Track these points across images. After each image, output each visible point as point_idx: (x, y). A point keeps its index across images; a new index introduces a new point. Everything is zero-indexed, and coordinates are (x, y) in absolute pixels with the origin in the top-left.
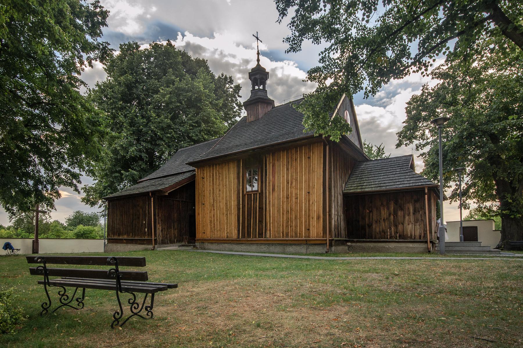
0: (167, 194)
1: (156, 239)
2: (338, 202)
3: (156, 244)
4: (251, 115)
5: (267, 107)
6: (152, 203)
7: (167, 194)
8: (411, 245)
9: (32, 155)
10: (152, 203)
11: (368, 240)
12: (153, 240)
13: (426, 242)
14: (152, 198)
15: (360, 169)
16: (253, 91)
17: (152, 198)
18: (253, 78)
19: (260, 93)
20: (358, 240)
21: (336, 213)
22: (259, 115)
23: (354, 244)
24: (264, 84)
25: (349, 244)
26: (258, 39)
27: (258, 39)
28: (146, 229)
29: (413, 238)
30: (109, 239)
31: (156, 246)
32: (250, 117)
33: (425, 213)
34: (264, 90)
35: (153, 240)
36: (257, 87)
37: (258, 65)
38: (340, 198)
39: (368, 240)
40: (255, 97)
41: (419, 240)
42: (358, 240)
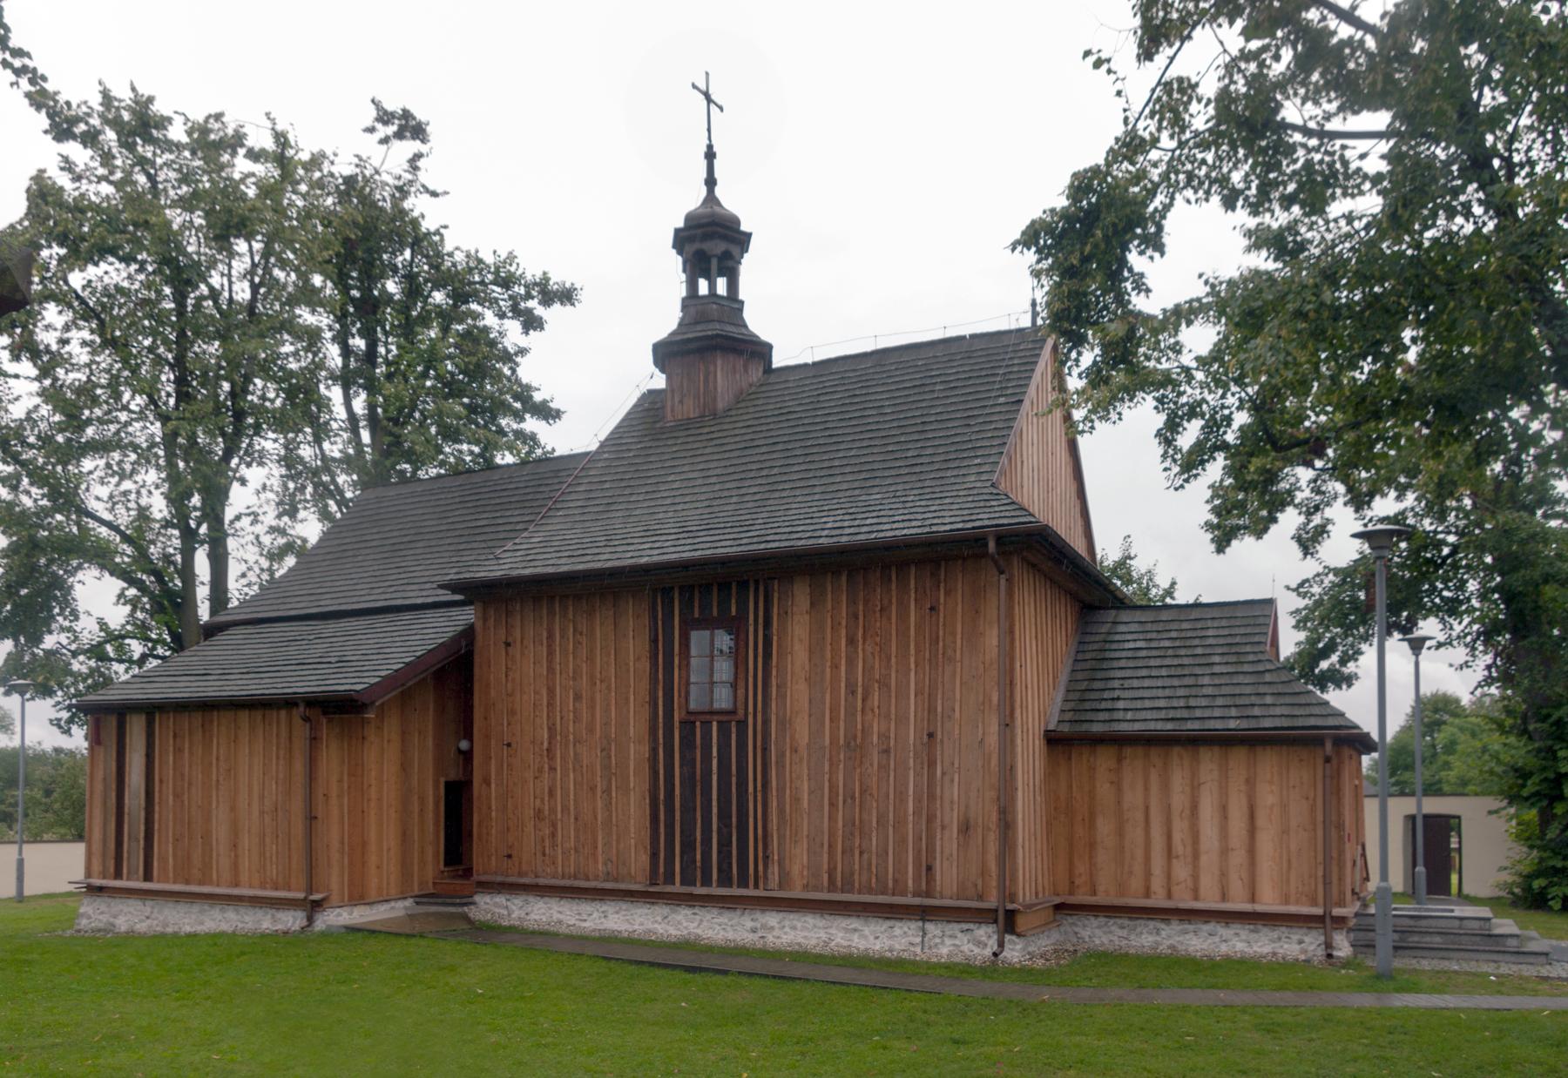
37: (711, 198)
40: (939, 830)
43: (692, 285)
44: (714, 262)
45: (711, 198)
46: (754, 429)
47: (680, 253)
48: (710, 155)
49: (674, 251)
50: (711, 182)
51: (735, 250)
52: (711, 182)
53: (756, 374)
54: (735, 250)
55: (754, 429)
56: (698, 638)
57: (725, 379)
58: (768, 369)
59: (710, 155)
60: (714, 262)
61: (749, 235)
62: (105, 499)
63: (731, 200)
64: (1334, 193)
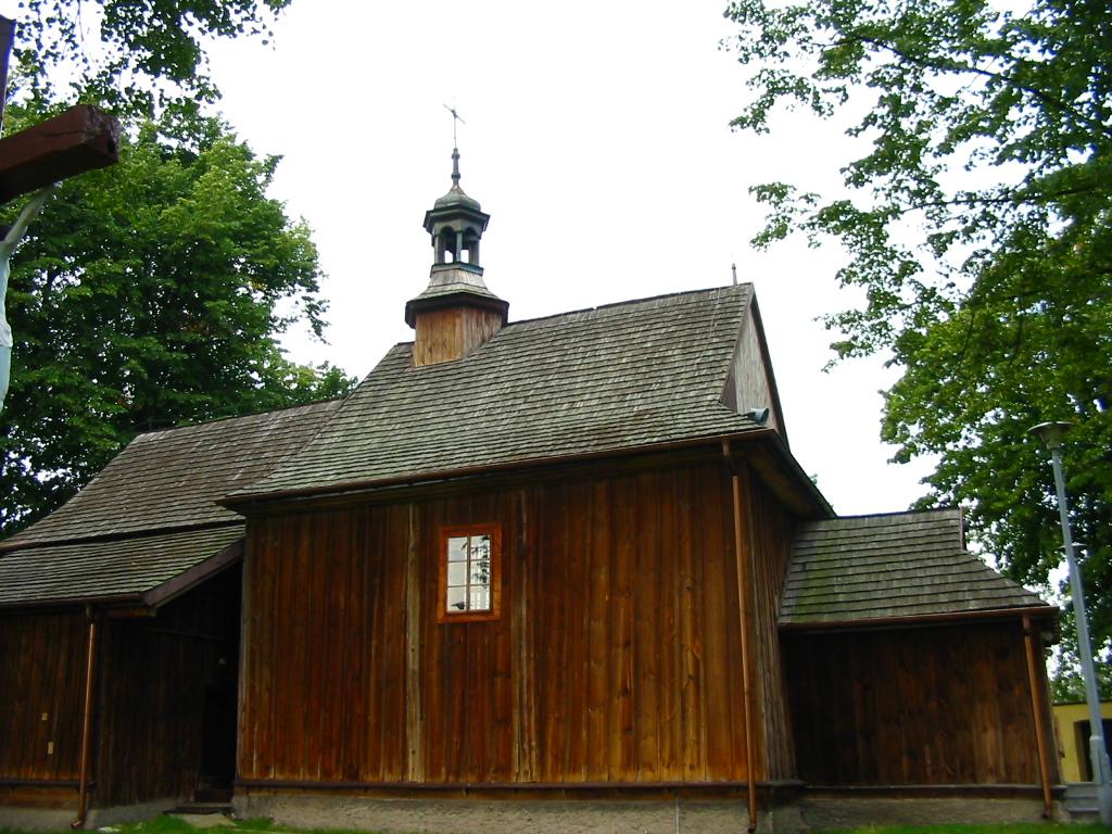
5: (487, 319)
18: (438, 227)
33: (1029, 693)
36: (449, 257)
37: (456, 189)
40: (449, 288)
43: (440, 255)
44: (459, 238)
45: (456, 189)
46: (395, 470)
47: (430, 231)
48: (456, 157)
49: (425, 229)
50: (456, 177)
51: (477, 228)
52: (456, 177)
53: (496, 324)
54: (477, 228)
55: (395, 470)
56: (455, 545)
57: (465, 331)
58: (505, 324)
59: (456, 157)
60: (459, 238)
61: (488, 217)
62: (960, 269)
63: (472, 190)
64: (1020, 95)
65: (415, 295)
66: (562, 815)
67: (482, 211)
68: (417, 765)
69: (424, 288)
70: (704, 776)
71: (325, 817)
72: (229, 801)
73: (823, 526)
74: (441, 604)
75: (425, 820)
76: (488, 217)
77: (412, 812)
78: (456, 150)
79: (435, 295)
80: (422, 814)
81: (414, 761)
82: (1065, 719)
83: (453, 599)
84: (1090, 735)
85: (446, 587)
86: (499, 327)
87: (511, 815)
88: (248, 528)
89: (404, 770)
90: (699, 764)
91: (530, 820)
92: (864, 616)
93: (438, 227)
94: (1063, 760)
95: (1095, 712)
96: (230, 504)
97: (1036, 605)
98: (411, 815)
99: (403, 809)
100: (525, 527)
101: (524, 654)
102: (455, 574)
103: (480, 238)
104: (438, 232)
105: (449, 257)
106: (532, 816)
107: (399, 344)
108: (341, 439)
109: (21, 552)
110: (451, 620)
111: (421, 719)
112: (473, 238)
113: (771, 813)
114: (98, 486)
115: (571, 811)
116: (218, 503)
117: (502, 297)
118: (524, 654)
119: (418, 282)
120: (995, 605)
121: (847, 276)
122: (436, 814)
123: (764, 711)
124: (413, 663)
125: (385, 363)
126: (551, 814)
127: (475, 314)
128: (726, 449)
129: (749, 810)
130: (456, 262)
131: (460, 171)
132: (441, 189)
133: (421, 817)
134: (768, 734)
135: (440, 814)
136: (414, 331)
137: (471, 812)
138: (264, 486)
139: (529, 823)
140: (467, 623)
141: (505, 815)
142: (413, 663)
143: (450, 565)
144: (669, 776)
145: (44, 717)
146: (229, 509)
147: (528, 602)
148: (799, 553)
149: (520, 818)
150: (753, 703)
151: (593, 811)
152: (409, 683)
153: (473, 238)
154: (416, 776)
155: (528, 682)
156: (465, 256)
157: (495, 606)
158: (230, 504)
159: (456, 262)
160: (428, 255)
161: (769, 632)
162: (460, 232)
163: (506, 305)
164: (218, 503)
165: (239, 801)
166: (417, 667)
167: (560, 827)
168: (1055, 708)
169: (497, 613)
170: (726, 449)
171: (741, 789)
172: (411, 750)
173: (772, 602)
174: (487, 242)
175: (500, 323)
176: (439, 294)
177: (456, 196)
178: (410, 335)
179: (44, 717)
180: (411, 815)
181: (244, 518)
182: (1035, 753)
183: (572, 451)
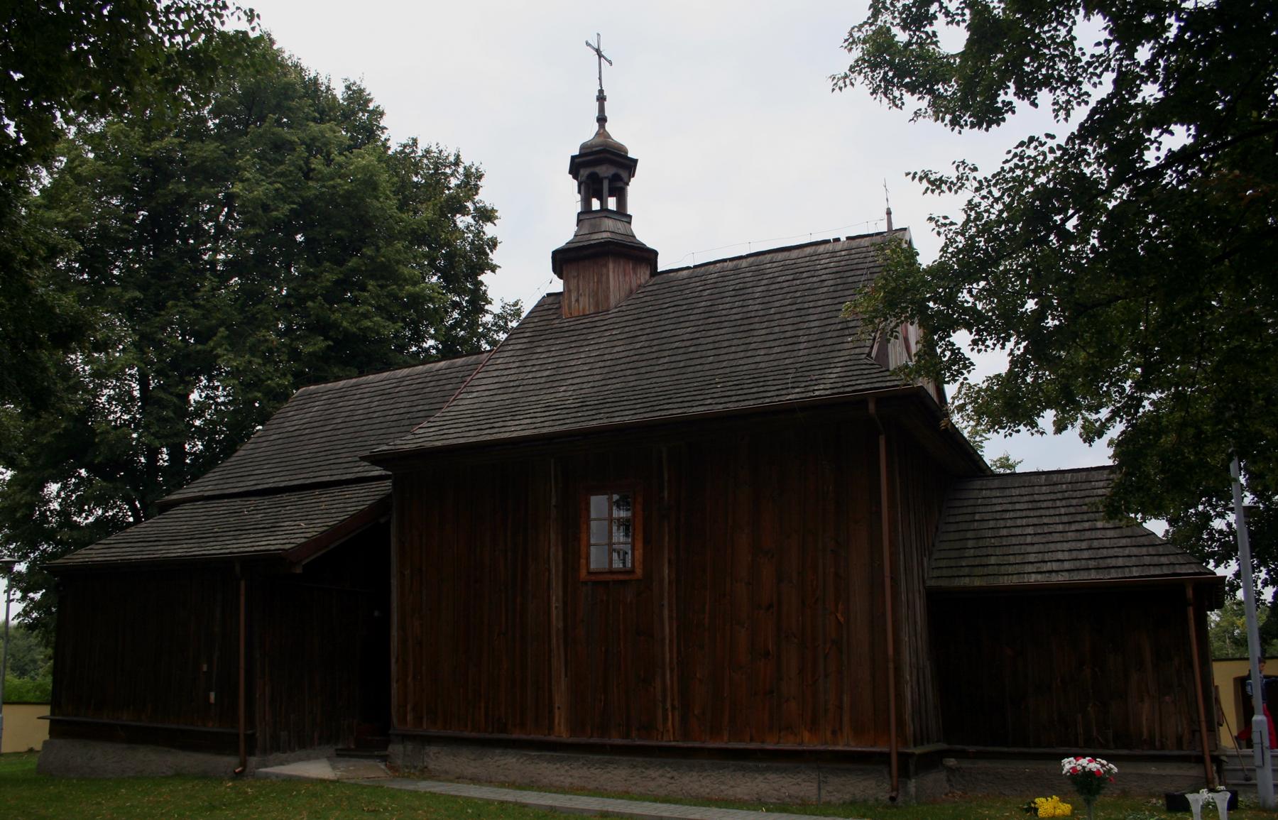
0: (299, 570)
1: (254, 735)
2: (915, 622)
3: (251, 751)
4: (579, 295)
5: (634, 269)
6: (242, 599)
7: (299, 570)
8: (1153, 769)
9: (233, 101)
10: (242, 599)
11: (1016, 750)
12: (242, 737)
13: (1200, 760)
14: (243, 584)
15: (966, 503)
16: (585, 214)
17: (243, 584)
18: (584, 173)
19: (609, 224)
20: (981, 748)
21: (914, 660)
22: (607, 298)
23: (966, 764)
24: (621, 196)
25: (951, 762)
26: (598, 51)
27: (598, 51)
28: (212, 696)
29: (1157, 743)
30: (58, 721)
31: (253, 760)
32: (577, 300)
33: (1191, 665)
34: (622, 214)
35: (242, 737)
36: (596, 204)
37: (602, 132)
38: (919, 604)
39: (1016, 750)
40: (595, 236)
41: (1176, 753)
42: (981, 748)
43: (586, 203)
44: (606, 185)
45: (602, 132)
47: (575, 177)
50: (602, 120)
51: (624, 174)
52: (602, 120)
53: (643, 275)
54: (624, 174)
59: (601, 98)
60: (606, 185)
61: (635, 162)
63: (618, 132)
65: (561, 243)
66: (705, 774)
67: (630, 155)
68: (563, 721)
69: (570, 237)
70: (846, 744)
71: (476, 768)
72: (386, 749)
73: (978, 484)
74: (583, 561)
75: (570, 773)
76: (635, 162)
77: (558, 765)
78: (601, 91)
79: (581, 244)
80: (567, 768)
81: (560, 718)
82: (1224, 676)
83: (597, 559)
84: (1253, 714)
85: (589, 545)
86: (647, 277)
87: (653, 773)
88: (394, 484)
89: (551, 728)
90: (841, 729)
91: (672, 778)
92: (1015, 580)
93: (584, 173)
94: (1221, 728)
95: (1257, 670)
96: (375, 459)
97: (1200, 574)
98: (557, 769)
99: (549, 762)
100: (666, 484)
101: (666, 613)
102: (597, 530)
103: (628, 184)
104: (584, 178)
105: (596, 204)
106: (675, 774)
107: (549, 295)
108: (832, 289)
109: (187, 506)
110: (593, 578)
111: (566, 676)
112: (620, 184)
113: (913, 780)
114: (260, 440)
115: (713, 771)
116: (363, 459)
117: (650, 245)
118: (666, 613)
119: (564, 232)
120: (1157, 573)
121: (387, 140)
122: (582, 768)
123: (908, 677)
124: (557, 622)
125: (533, 315)
126: (694, 774)
127: (622, 263)
128: (872, 407)
129: (891, 777)
130: (604, 209)
131: (607, 114)
132: (588, 132)
133: (567, 771)
134: (912, 700)
135: (585, 768)
136: (562, 281)
137: (615, 768)
138: (407, 443)
139: (673, 781)
140: (608, 583)
141: (648, 772)
142: (557, 622)
143: (592, 522)
144: (810, 742)
145: (205, 668)
146: (373, 464)
147: (669, 561)
148: (952, 519)
149: (662, 776)
150: (898, 670)
151: (734, 771)
152: (554, 641)
153: (620, 184)
154: (562, 732)
155: (671, 641)
156: (612, 203)
157: (637, 564)
158: (375, 459)
159: (604, 209)
160: (573, 202)
161: (917, 595)
162: (606, 178)
163: (655, 253)
164: (363, 459)
165: (395, 749)
166: (561, 625)
167: (702, 786)
168: (1214, 663)
169: (639, 572)
170: (872, 407)
171: (884, 758)
172: (557, 705)
173: (921, 564)
174: (634, 189)
175: (648, 273)
176: (585, 243)
177: (600, 140)
178: (558, 286)
179: (205, 668)
180: (557, 769)
181: (390, 473)
182: (1197, 734)
183: (728, 405)
